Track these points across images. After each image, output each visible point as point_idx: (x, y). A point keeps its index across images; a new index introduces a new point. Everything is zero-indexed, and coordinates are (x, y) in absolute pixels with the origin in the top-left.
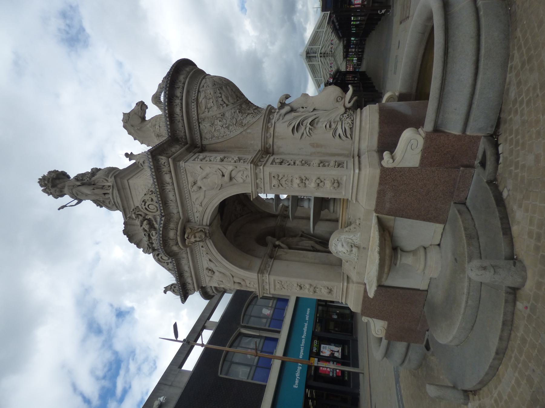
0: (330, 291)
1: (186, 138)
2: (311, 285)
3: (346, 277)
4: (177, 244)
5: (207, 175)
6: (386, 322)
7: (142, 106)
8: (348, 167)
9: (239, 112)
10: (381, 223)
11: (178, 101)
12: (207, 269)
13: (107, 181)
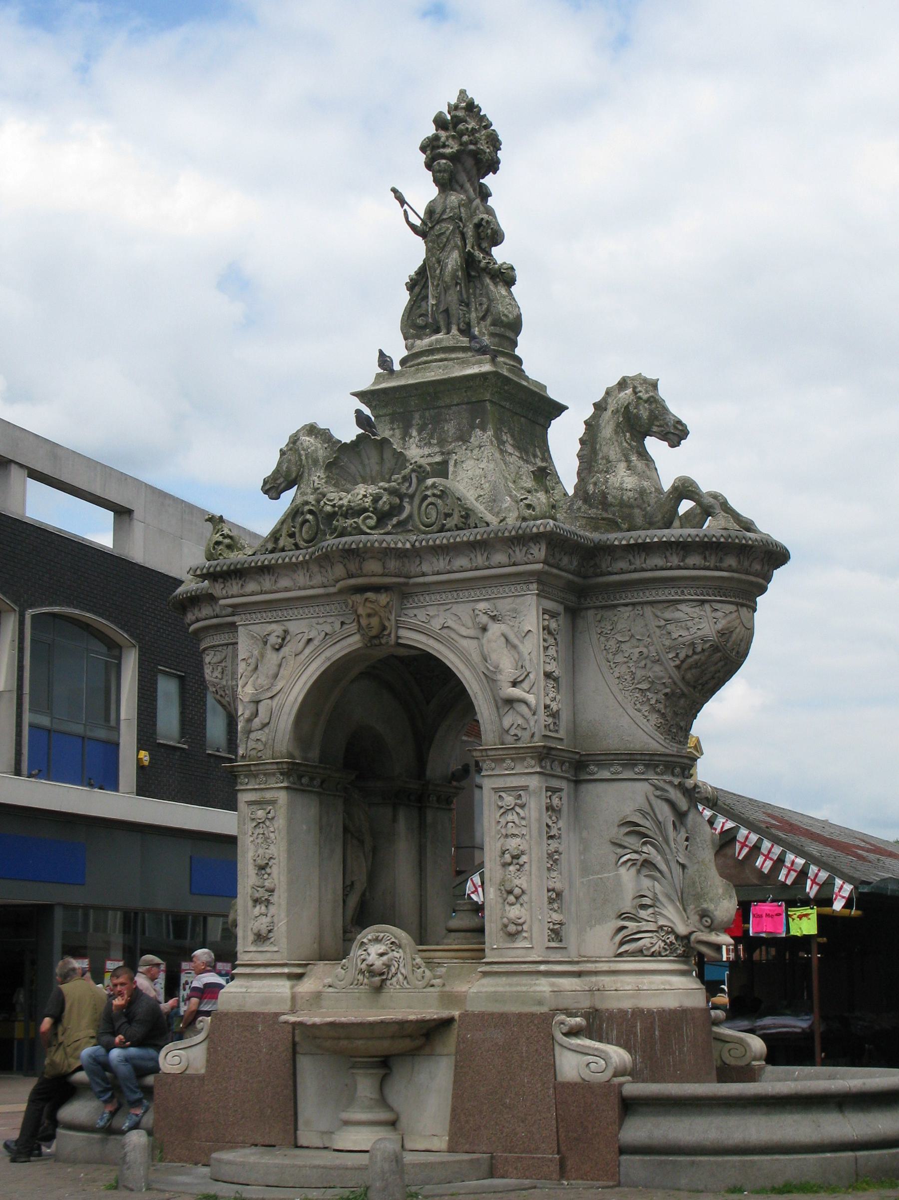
0: (261, 938)
1: (597, 575)
2: (272, 891)
3: (299, 970)
4: (351, 576)
5: (514, 647)
6: (203, 1071)
7: (676, 434)
8: (550, 952)
9: (666, 694)
10: (427, 1035)
11: (675, 560)
12: (286, 632)
13: (483, 318)
